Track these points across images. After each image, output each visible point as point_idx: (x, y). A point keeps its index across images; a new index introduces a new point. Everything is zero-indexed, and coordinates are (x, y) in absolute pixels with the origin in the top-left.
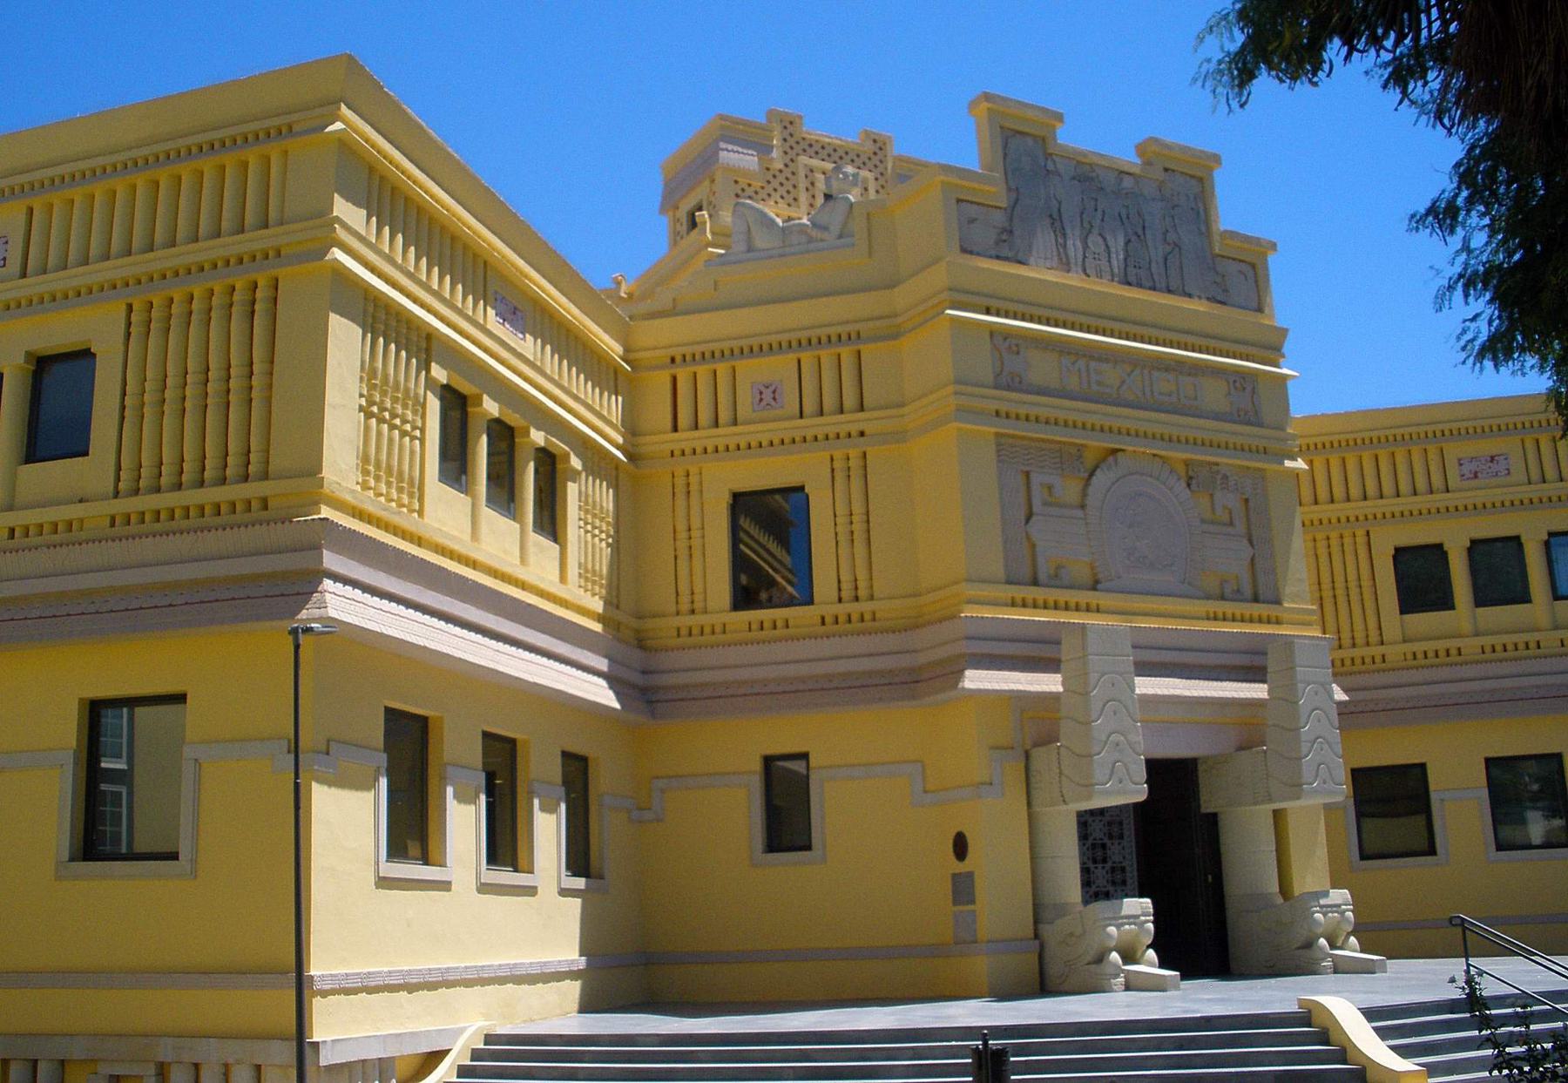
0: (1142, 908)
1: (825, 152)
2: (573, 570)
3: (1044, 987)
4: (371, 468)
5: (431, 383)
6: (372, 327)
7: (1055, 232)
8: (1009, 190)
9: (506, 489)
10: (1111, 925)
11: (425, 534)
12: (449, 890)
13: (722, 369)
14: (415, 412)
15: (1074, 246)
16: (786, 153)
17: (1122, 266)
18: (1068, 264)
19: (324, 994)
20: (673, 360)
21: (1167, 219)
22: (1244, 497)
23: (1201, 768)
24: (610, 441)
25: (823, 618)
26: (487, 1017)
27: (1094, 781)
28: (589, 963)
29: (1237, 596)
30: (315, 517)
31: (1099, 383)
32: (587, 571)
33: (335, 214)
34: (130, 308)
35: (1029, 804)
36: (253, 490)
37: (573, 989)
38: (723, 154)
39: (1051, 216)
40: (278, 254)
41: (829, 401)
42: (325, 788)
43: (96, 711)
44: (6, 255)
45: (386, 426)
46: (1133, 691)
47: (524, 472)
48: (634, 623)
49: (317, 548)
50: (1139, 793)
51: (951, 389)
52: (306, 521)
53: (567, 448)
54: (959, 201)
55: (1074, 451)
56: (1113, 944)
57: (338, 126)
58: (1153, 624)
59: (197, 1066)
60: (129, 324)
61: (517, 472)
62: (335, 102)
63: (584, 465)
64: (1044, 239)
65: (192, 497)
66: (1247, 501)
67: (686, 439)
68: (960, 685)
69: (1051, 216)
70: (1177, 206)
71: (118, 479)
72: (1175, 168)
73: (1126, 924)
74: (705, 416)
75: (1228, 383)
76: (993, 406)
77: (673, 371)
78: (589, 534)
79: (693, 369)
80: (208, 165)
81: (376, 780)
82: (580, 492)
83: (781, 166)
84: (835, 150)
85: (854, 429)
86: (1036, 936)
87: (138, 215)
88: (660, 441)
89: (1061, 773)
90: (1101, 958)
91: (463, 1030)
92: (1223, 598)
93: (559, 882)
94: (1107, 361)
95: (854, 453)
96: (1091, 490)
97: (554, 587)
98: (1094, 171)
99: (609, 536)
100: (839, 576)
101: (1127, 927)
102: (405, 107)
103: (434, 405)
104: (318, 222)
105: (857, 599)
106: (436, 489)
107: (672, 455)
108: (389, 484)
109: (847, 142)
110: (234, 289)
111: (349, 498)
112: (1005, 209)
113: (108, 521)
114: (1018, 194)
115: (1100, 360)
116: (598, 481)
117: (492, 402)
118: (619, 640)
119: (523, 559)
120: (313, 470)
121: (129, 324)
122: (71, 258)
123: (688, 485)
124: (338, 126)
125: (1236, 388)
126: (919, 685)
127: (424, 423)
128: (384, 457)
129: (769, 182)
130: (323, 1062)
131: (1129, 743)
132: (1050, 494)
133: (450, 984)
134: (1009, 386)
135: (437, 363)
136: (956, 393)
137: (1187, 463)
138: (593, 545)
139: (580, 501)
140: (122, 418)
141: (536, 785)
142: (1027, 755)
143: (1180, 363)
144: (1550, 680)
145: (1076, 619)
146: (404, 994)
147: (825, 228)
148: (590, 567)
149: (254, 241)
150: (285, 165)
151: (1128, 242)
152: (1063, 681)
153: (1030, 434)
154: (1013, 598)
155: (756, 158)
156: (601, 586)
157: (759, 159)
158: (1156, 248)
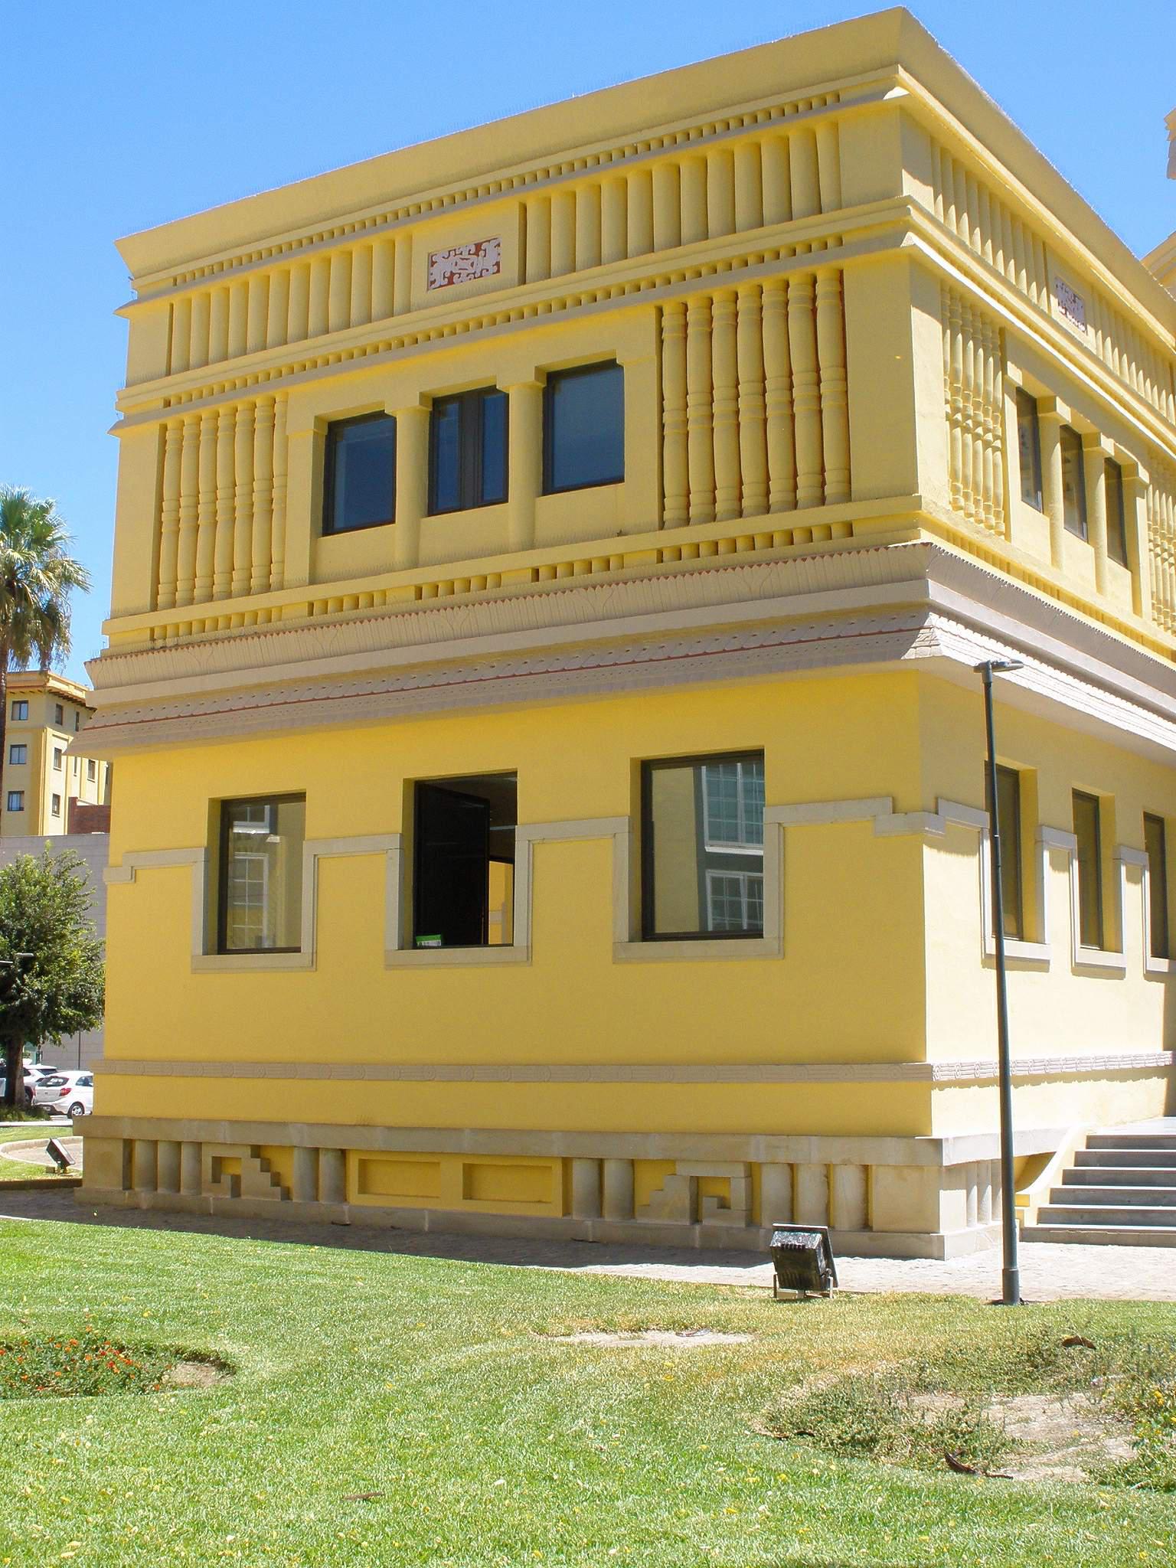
5: (1007, 383)
6: (951, 323)
9: (1076, 504)
14: (995, 421)
19: (942, 1086)
30: (914, 542)
33: (905, 193)
34: (660, 312)
36: (834, 514)
37: (1158, 1087)
43: (227, 811)
45: (970, 435)
49: (919, 578)
52: (905, 546)
57: (897, 92)
60: (660, 331)
62: (891, 64)
65: (778, 522)
71: (663, 508)
78: (1159, 558)
80: (739, 145)
81: (980, 843)
103: (1011, 409)
104: (885, 203)
106: (1021, 510)
108: (977, 502)
110: (788, 285)
113: (654, 556)
117: (1064, 405)
120: (906, 489)
130: (945, 1163)
133: (1051, 1078)
138: (1164, 570)
139: (1149, 520)
140: (662, 438)
141: (1124, 850)
149: (807, 229)
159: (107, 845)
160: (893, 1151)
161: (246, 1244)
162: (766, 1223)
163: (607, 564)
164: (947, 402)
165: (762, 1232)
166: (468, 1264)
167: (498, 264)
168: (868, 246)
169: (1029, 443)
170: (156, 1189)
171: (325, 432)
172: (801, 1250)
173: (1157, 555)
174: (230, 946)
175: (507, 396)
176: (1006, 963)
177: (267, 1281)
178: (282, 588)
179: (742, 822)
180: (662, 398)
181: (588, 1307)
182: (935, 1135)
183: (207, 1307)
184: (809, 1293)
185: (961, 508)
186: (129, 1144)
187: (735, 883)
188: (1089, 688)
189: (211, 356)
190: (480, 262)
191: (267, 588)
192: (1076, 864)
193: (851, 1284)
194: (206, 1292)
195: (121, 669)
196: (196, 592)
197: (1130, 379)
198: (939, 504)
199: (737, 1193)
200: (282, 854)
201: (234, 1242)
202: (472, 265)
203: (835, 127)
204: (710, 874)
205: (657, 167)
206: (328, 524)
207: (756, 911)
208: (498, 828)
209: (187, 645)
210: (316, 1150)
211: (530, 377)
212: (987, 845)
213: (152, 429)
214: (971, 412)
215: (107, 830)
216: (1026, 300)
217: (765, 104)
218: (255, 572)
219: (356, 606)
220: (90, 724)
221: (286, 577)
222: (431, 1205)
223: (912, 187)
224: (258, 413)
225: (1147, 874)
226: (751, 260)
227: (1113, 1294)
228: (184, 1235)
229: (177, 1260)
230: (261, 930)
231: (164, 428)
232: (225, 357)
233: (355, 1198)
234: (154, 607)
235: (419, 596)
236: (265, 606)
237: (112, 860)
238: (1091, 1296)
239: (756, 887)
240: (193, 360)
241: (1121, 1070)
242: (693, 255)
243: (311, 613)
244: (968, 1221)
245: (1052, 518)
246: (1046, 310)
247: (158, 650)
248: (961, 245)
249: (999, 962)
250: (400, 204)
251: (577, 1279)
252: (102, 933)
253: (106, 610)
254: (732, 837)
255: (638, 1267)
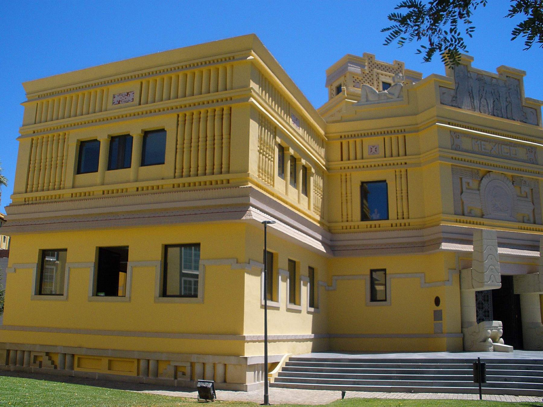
0: (499, 324)
1: (383, 67)
2: (312, 206)
3: (464, 350)
4: (261, 171)
5: (276, 142)
7: (470, 98)
8: (456, 83)
10: (489, 329)
11: (275, 193)
12: (279, 310)
13: (358, 140)
14: (272, 152)
15: (477, 103)
16: (369, 68)
17: (492, 109)
18: (475, 108)
19: (248, 342)
20: (341, 137)
21: (507, 94)
22: (531, 188)
23: (514, 279)
24: (322, 162)
25: (392, 225)
26: (288, 352)
27: (484, 281)
28: (315, 336)
29: (528, 222)
30: (247, 186)
31: (485, 149)
32: (315, 207)
33: (251, 86)
34: (178, 116)
35: (460, 289)
36: (227, 176)
37: (310, 344)
38: (349, 67)
39: (469, 92)
40: (231, 99)
41: (395, 152)
42: (248, 275)
43: (44, 253)
44: (134, 97)
46: (497, 252)
47: (299, 174)
48: (328, 225)
49: (247, 196)
50: (498, 286)
51: (438, 149)
53: (311, 166)
54: (440, 86)
55: (476, 171)
56: (489, 335)
57: (251, 57)
58: (502, 230)
59: (204, 364)
61: (297, 172)
62: (249, 50)
63: (315, 172)
64: (467, 101)
66: (532, 189)
67: (346, 163)
68: (440, 248)
69: (469, 92)
70: (511, 89)
71: (175, 172)
72: (510, 76)
73: (494, 329)
74: (352, 156)
75: (527, 149)
76: (451, 155)
77: (341, 141)
78: (316, 194)
79: (348, 140)
80: (205, 70)
81: (261, 273)
82: (314, 180)
83: (368, 72)
84: (382, 66)
85: (403, 162)
86: (462, 332)
88: (337, 164)
89: (472, 278)
90: (485, 340)
91: (282, 356)
92: (524, 222)
94: (487, 141)
95: (403, 170)
96: (481, 185)
97: (308, 212)
98: (483, 77)
99: (321, 195)
100: (397, 211)
101: (494, 330)
102: (269, 51)
103: (277, 150)
104: (245, 89)
105: (403, 218)
106: (277, 178)
107: (341, 169)
108: (265, 176)
109: (389, 64)
111: (256, 180)
112: (454, 89)
113: (172, 186)
114: (459, 84)
115: (485, 141)
116: (319, 177)
118: (324, 229)
119: (299, 202)
120: (245, 170)
121: (178, 121)
122: (156, 99)
123: (346, 179)
124: (251, 57)
125: (529, 151)
126: (425, 247)
127: (274, 156)
129: (364, 77)
130: (248, 364)
131: (496, 269)
132: (468, 185)
133: (279, 341)
134: (456, 149)
135: (278, 136)
136: (440, 151)
137: (512, 176)
140: (176, 152)
142: (460, 272)
143: (511, 143)
145: (476, 227)
146: (257, 343)
147: (393, 94)
148: (316, 205)
150: (232, 71)
151: (494, 101)
152: (473, 248)
153: (462, 165)
154: (456, 220)
155: (360, 69)
156: (319, 211)
157: (361, 69)
158: (503, 103)
159: (7, 262)
160: (233, 360)
161: (43, 382)
162: (196, 379)
163: (153, 188)
164: (258, 147)
165: (195, 382)
166: (109, 389)
167: (133, 99)
168: (239, 101)
169: (281, 158)
170: (16, 365)
171: (143, 135)
172: (206, 388)
173: (316, 193)
174: (42, 293)
175: (133, 137)
176: (267, 307)
177: (48, 393)
178: (64, 189)
179: (193, 264)
180: (177, 141)
181: (143, 403)
182: (245, 356)
183: (29, 401)
184: (208, 400)
185: (261, 177)
186: (8, 351)
187: (190, 282)
188: (294, 230)
189: (83, 113)
190: (128, 98)
191: (60, 189)
192: (288, 280)
193: (220, 398)
194: (29, 396)
195: (14, 209)
196: (56, 186)
197: (311, 143)
198: (254, 175)
199: (188, 370)
200: (59, 267)
201: (39, 381)
202: (126, 98)
204: (183, 279)
205: (181, 74)
206: (79, 171)
207: (196, 290)
208: (123, 262)
209: (35, 204)
210: (65, 354)
211: (106, 137)
212: (263, 273)
213: (30, 139)
214: (265, 150)
215: (8, 257)
216: (283, 119)
217: (210, 59)
218: (56, 183)
219: (85, 195)
220: (5, 225)
221: (65, 186)
222: (98, 371)
223: (253, 85)
224: (60, 137)
225: (309, 284)
226: (187, 106)
227: (296, 403)
228: (24, 379)
229: (21, 387)
230: (52, 289)
231: (33, 140)
232: (57, 119)
233: (76, 369)
234: (26, 192)
235: (104, 193)
236: (28, 197)
237: (9, 266)
238: (289, 403)
239: (196, 283)
240: (43, 120)
241: (307, 339)
242: (189, 100)
243: (72, 197)
244: (254, 381)
245: (286, 180)
246: (288, 122)
247: (27, 204)
248: (265, 102)
249: (265, 307)
250: (161, 68)
251: (140, 394)
252: (5, 287)
253: (12, 192)
254: (190, 268)
255: (158, 391)
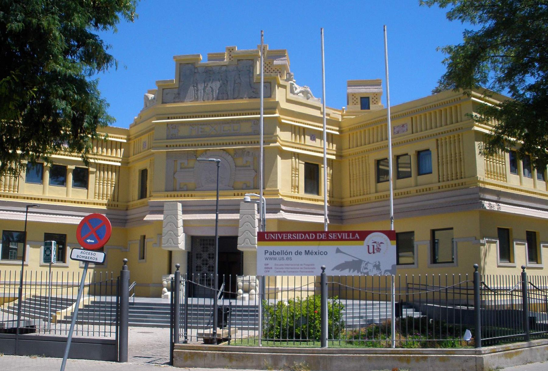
36: (463, 180)
87: (418, 126)
93: (498, 264)
115: (201, 125)
127: (505, 160)
128: (498, 171)
144: (410, 205)
171: (376, 162)
203: (460, 105)
206: (378, 181)
211: (414, 153)
